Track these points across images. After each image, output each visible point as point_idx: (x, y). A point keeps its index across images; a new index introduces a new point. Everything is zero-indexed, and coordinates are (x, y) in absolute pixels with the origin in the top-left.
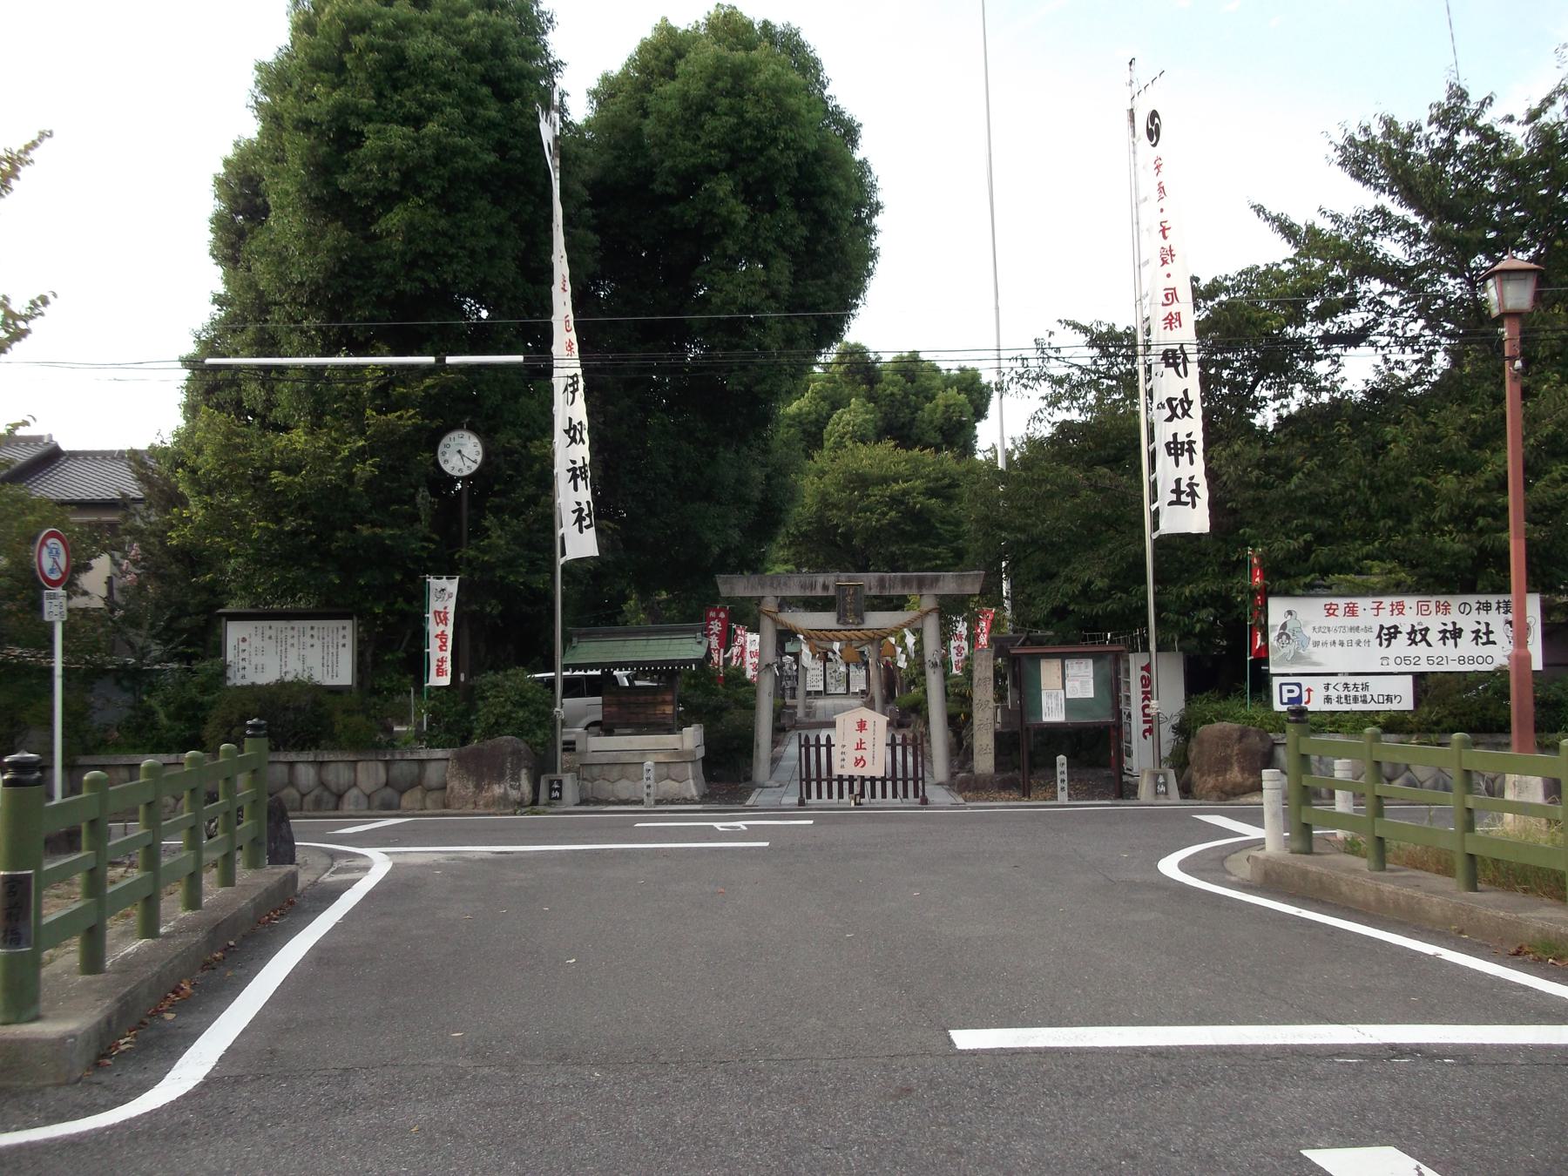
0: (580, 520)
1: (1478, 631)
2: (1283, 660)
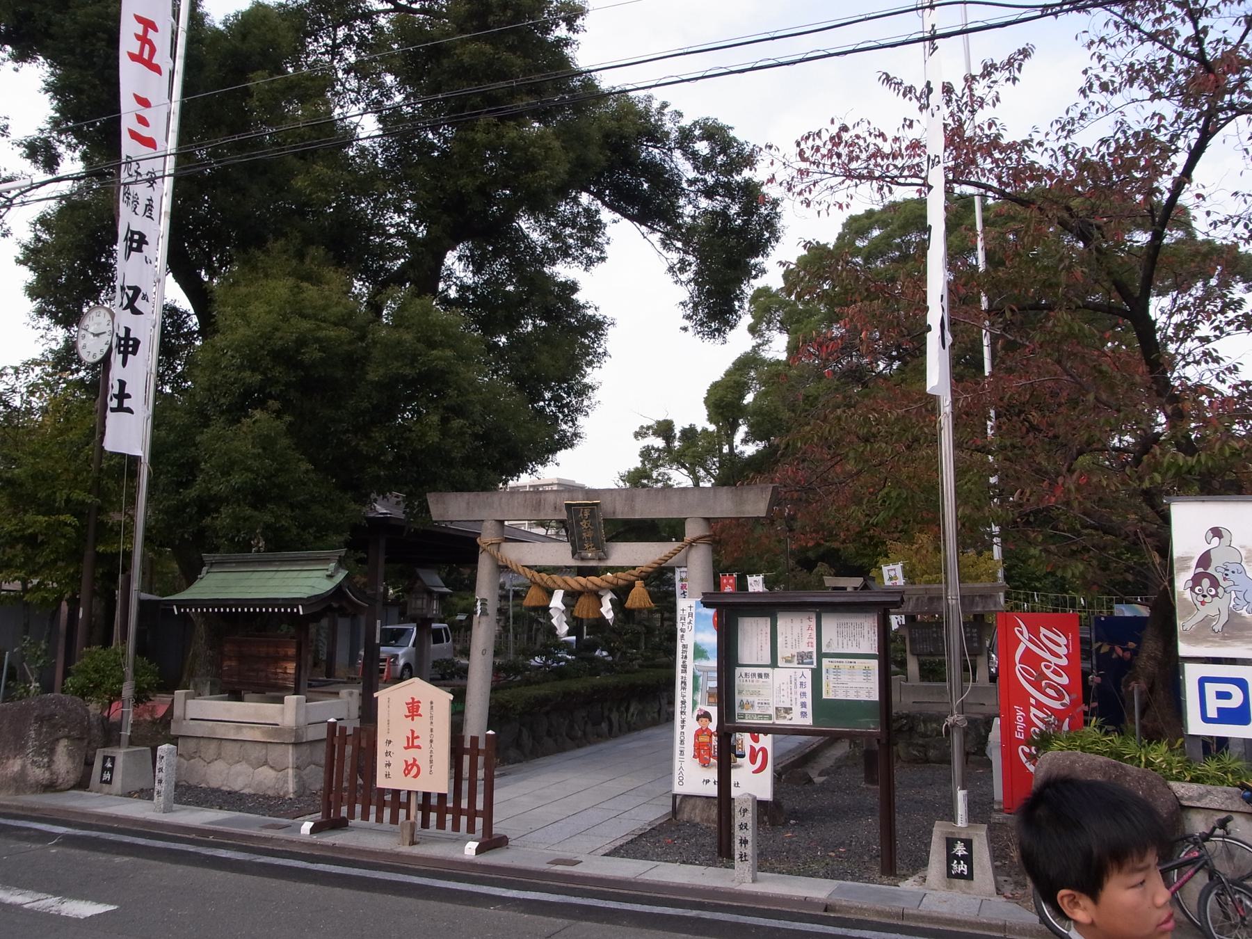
2: (1204, 631)
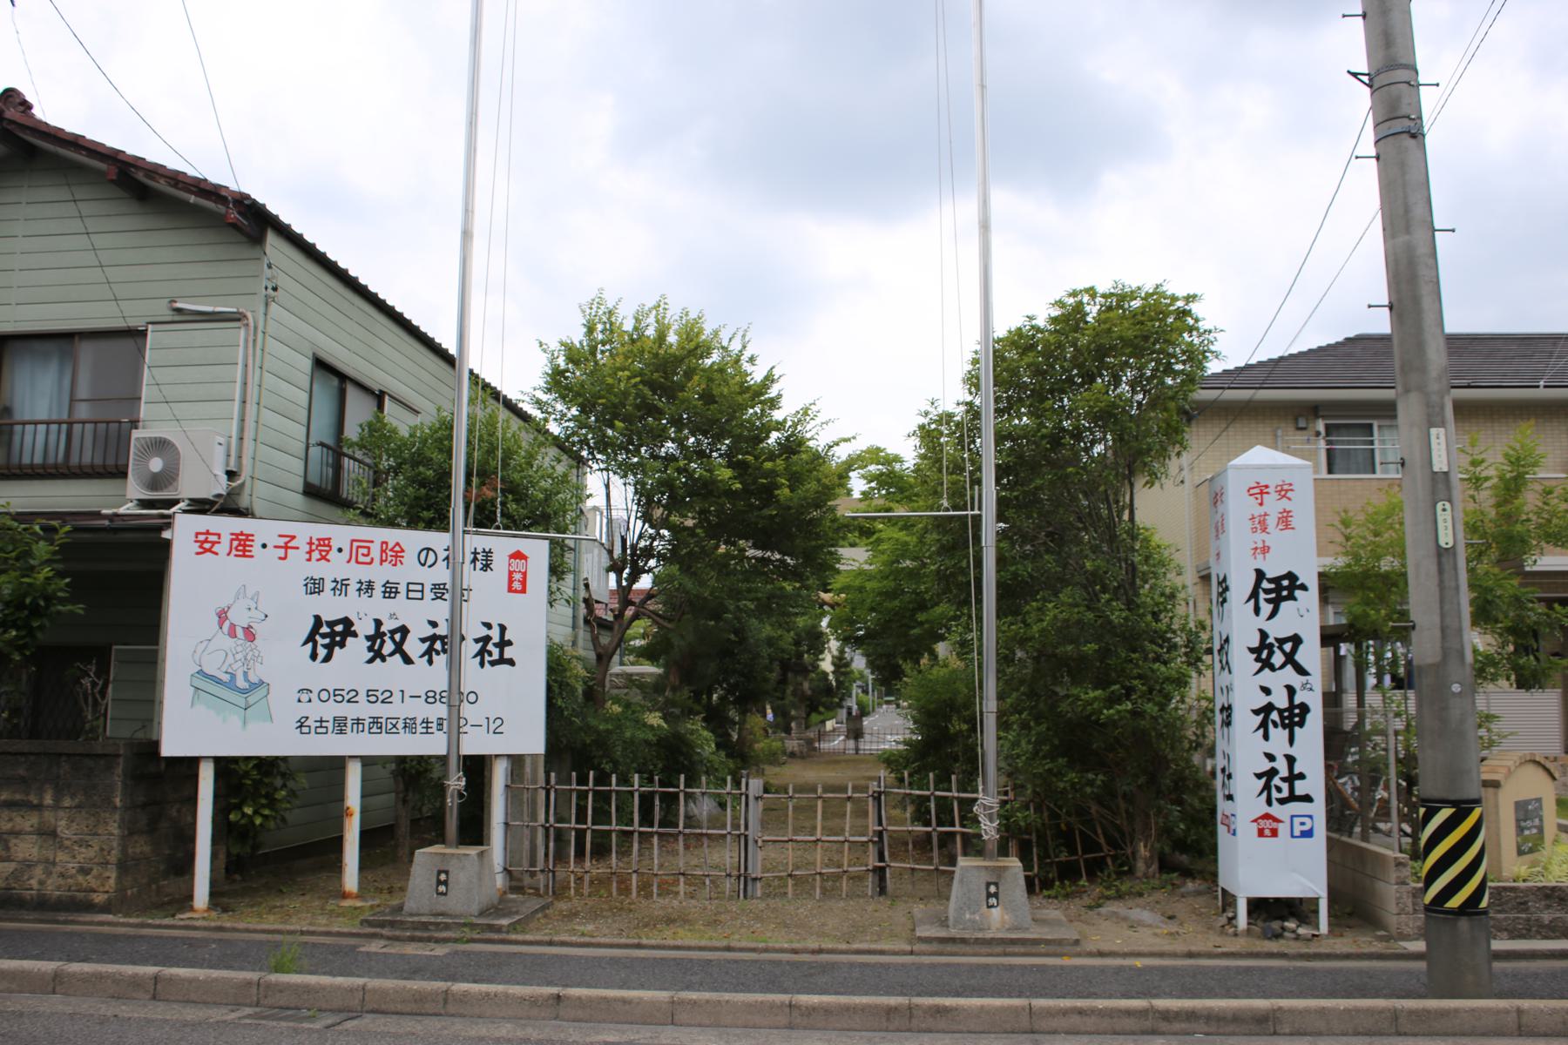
0: (474, 560)
1: (487, 639)
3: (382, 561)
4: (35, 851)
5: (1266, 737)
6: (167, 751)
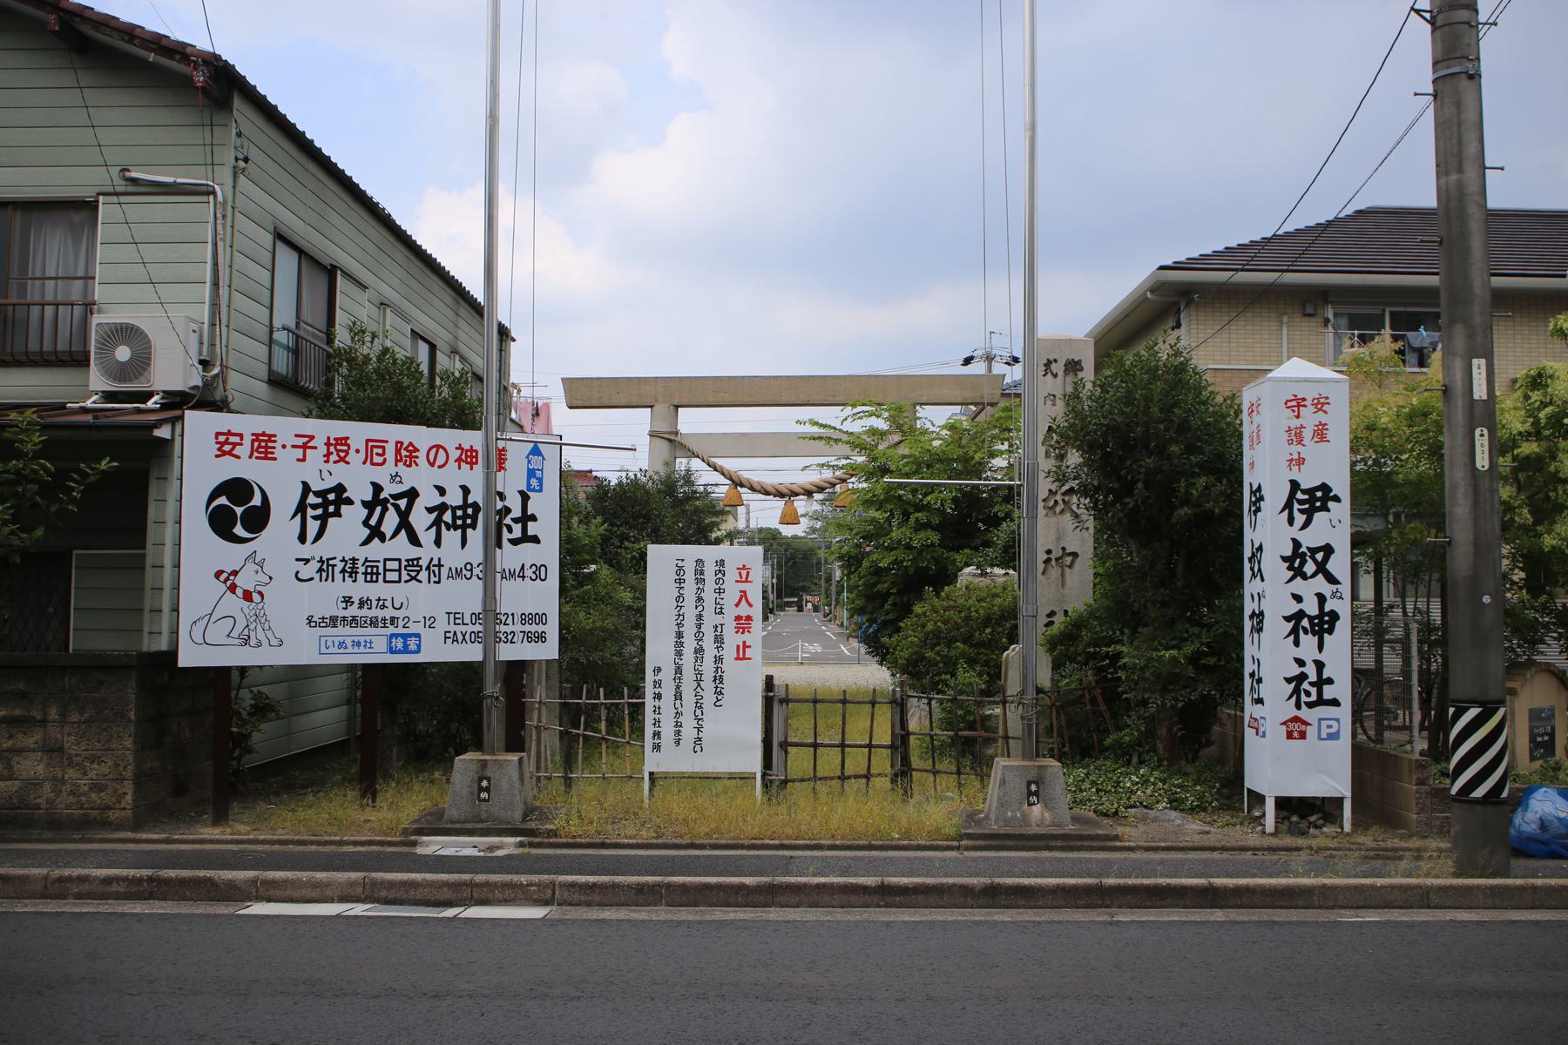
3: (397, 461)
4: (41, 769)
5: (1297, 643)
6: (180, 665)
